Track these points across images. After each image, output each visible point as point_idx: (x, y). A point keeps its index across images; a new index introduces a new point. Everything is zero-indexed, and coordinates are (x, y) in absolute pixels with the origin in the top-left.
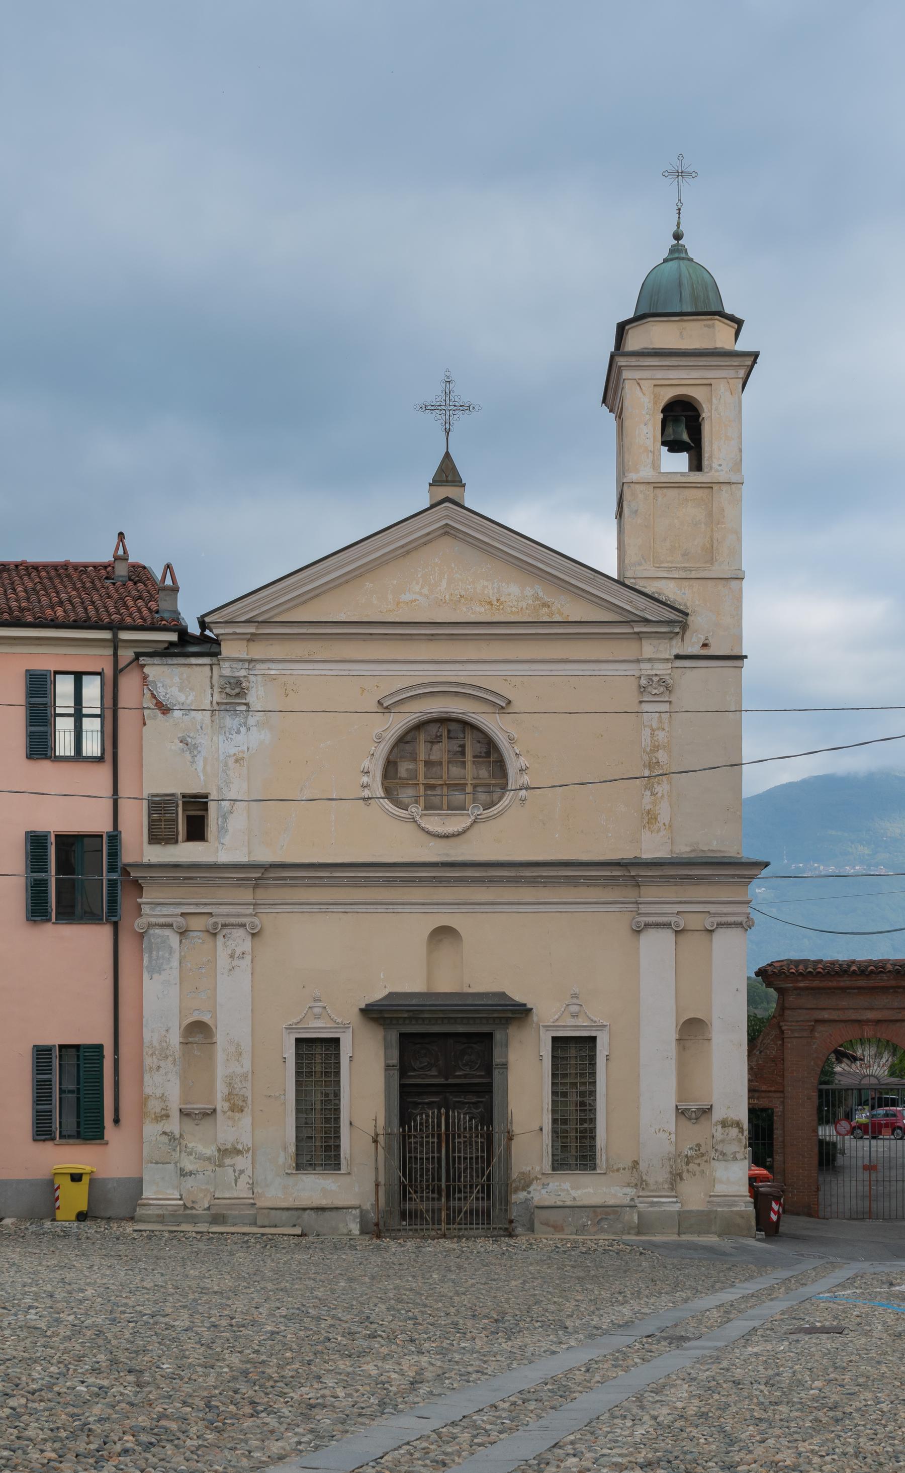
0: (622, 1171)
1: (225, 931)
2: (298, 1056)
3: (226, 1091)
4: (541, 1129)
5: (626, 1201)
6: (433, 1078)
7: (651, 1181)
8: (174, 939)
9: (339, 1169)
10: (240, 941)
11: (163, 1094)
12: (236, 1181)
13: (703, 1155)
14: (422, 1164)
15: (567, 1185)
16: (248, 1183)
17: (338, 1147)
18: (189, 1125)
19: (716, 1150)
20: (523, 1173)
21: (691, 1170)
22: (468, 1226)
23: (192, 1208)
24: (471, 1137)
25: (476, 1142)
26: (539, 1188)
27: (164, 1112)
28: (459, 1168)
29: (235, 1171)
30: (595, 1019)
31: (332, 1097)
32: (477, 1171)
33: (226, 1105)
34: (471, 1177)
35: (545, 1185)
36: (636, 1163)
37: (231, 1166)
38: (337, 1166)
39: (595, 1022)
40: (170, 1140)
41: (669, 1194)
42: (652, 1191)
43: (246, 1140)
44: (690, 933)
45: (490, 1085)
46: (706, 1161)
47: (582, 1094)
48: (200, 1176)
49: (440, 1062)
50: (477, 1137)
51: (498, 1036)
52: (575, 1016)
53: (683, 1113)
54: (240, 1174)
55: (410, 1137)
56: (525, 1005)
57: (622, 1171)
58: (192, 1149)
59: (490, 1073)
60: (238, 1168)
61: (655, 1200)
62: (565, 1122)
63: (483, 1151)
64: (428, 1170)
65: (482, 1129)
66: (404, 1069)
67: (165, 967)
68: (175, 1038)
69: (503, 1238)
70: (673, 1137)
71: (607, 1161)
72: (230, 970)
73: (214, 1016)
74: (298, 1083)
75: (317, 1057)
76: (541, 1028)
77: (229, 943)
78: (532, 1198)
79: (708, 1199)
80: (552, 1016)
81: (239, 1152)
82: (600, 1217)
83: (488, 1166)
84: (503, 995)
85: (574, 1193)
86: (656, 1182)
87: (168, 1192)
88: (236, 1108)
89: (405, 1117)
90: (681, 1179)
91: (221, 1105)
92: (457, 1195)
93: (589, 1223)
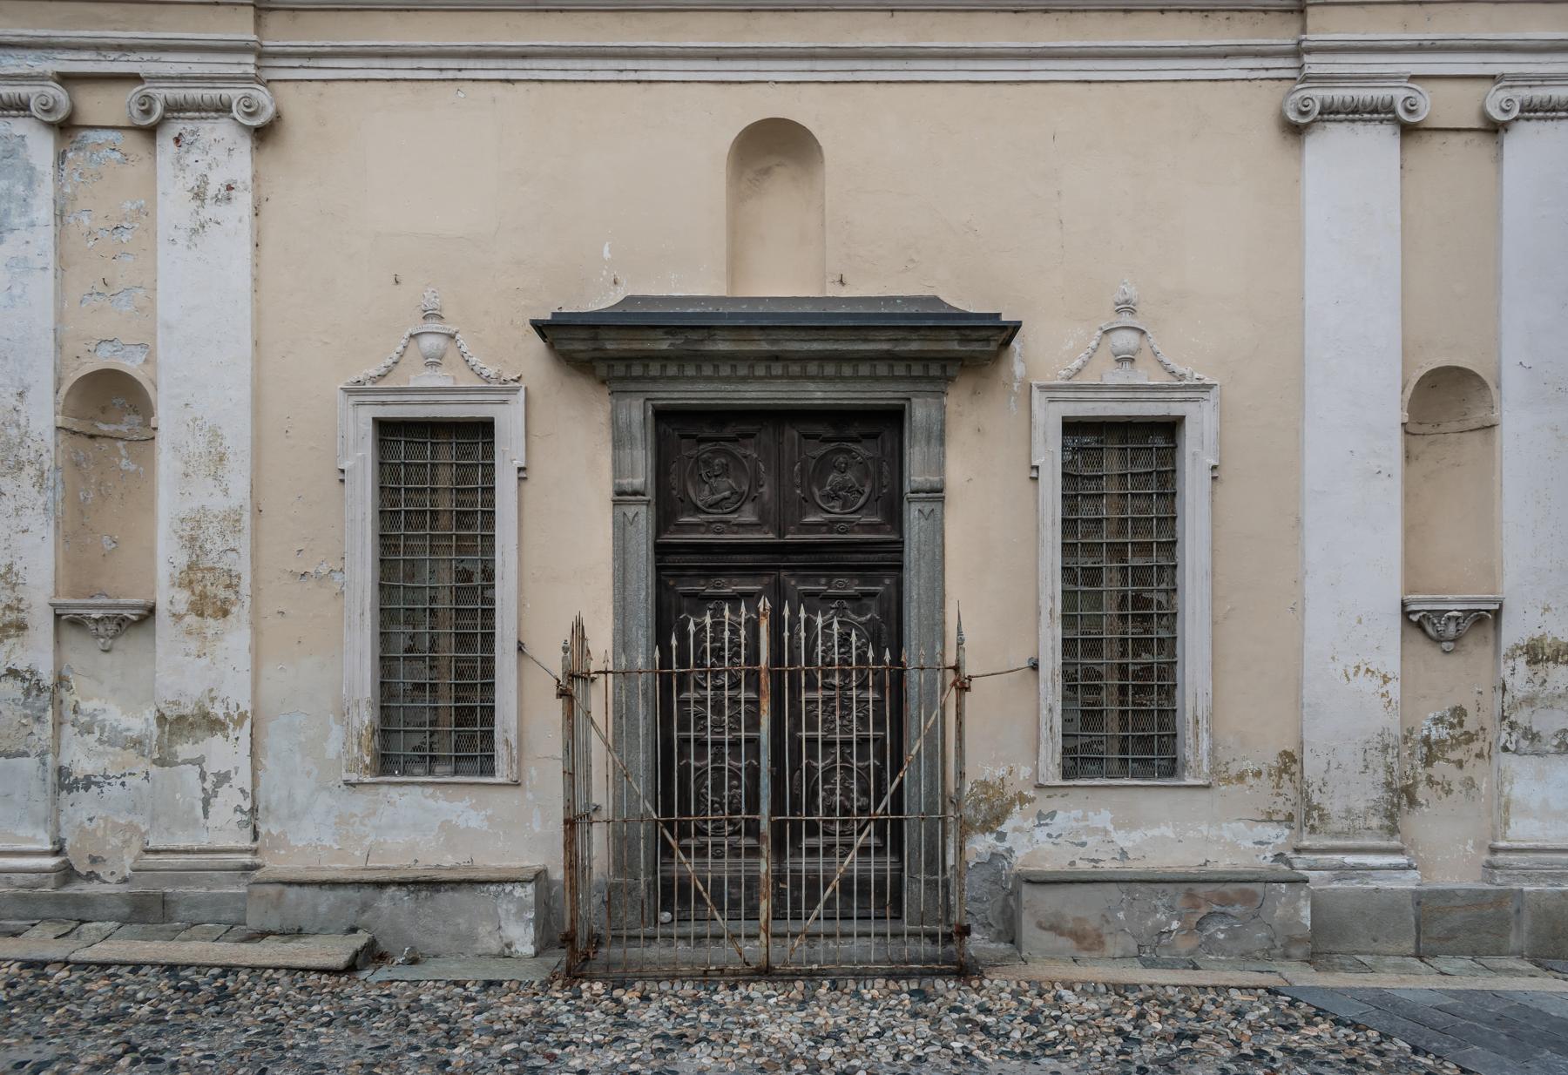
0: (1250, 780)
1: (176, 128)
2: (385, 468)
3: (182, 559)
4: (1035, 667)
5: (1264, 861)
6: (746, 525)
7: (1334, 806)
8: (41, 147)
9: (492, 773)
10: (220, 150)
11: (10, 567)
12: (206, 804)
13: (1470, 738)
14: (718, 757)
15: (1103, 818)
16: (238, 809)
17: (489, 712)
18: (82, 653)
19: (1512, 725)
20: (985, 784)
21: (1438, 778)
22: (839, 926)
23: (91, 877)
24: (845, 687)
25: (862, 702)
26: (1028, 824)
27: (11, 616)
28: (811, 770)
29: (203, 777)
30: (1180, 369)
31: (478, 580)
32: (863, 780)
33: (183, 597)
34: (846, 792)
35: (1043, 818)
36: (1289, 762)
37: (192, 762)
38: (1171, 768)
39: (1183, 376)
40: (27, 693)
41: (1384, 844)
42: (1337, 835)
43: (236, 693)
44: (1438, 138)
45: (896, 548)
46: (1479, 756)
47: (1141, 575)
48: (113, 791)
49: (764, 489)
50: (863, 686)
51: (920, 412)
52: (1125, 359)
53: (1419, 625)
54: (217, 785)
55: (683, 686)
56: (998, 315)
57: (1250, 780)
58: (93, 716)
59: (894, 514)
60: (212, 767)
61: (1350, 859)
62: (1093, 647)
63: (880, 724)
64: (735, 775)
65: (879, 659)
66: (667, 505)
67: (15, 221)
68: (42, 417)
69: (940, 984)
70: (1394, 689)
71: (1213, 752)
72: (195, 231)
73: (148, 349)
74: (386, 543)
75: (433, 468)
76: (1036, 393)
77: (190, 159)
78: (1010, 850)
79: (1486, 857)
80: (1064, 357)
81: (215, 725)
82: (1204, 911)
83: (898, 766)
84: (936, 300)
85: (1123, 839)
86: (1349, 811)
87: (21, 833)
88: (210, 606)
89: (665, 623)
90: (1413, 802)
91: (168, 597)
92: (805, 842)
93: (1175, 925)
